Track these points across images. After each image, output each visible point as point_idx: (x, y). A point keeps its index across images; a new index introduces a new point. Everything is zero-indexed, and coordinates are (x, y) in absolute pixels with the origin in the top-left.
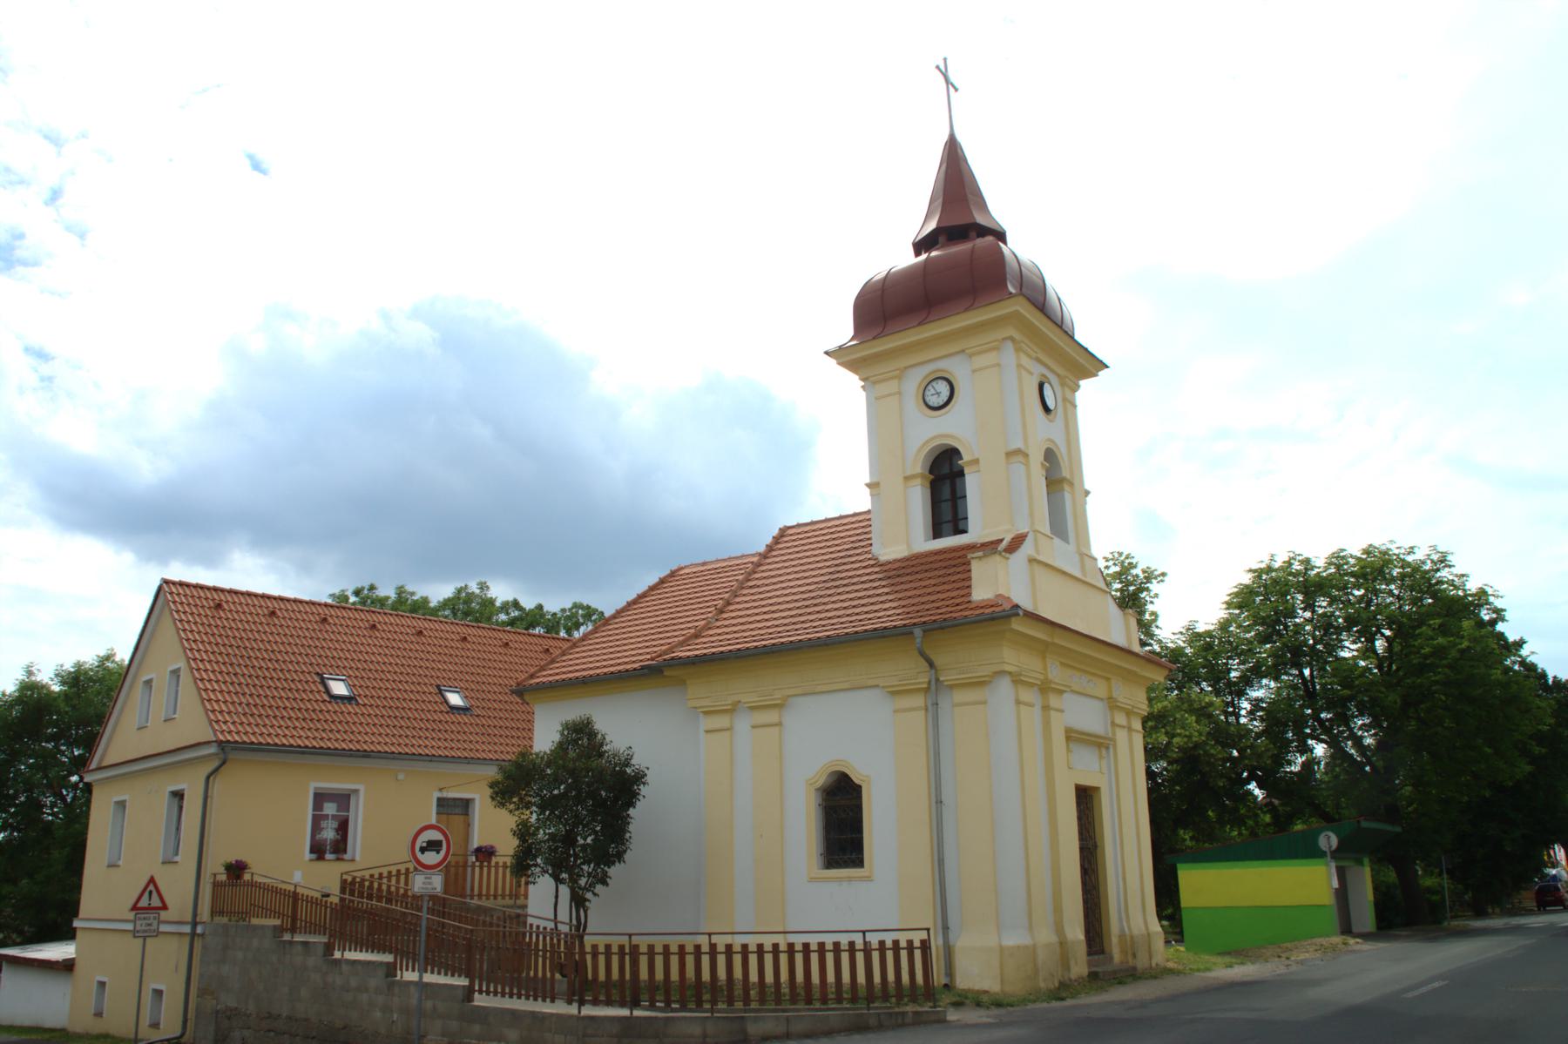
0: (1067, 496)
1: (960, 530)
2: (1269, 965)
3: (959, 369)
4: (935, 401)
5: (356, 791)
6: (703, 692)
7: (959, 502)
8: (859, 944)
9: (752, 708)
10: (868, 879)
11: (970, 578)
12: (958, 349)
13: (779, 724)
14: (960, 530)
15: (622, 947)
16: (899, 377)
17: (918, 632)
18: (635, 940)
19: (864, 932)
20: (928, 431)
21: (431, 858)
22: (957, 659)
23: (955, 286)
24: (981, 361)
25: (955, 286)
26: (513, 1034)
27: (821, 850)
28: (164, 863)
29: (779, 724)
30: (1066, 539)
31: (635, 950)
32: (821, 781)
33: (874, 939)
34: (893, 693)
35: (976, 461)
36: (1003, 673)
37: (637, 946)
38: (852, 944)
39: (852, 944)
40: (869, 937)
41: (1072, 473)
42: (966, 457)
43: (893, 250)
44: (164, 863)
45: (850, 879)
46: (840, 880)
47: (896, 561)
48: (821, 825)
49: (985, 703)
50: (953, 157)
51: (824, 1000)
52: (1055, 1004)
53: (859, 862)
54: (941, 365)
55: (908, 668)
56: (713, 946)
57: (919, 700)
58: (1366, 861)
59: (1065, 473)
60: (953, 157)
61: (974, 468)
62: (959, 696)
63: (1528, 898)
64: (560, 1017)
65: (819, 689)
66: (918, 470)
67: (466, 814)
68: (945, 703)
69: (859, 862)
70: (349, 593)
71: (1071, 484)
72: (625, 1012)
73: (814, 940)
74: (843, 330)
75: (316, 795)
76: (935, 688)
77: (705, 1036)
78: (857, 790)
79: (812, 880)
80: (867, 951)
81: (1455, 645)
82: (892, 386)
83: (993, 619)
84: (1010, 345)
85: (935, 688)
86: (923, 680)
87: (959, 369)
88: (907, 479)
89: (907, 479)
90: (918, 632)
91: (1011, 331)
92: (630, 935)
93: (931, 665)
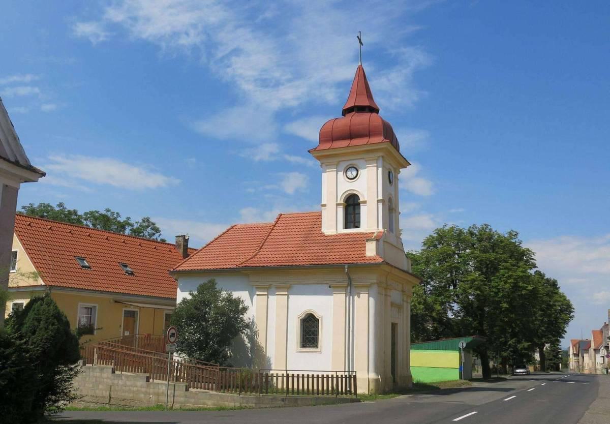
0: (394, 215)
1: (357, 226)
2: (161, 385)
4: (351, 176)
5: (95, 307)
7: (357, 216)
8: (335, 376)
12: (362, 157)
14: (357, 226)
19: (336, 372)
21: (172, 339)
30: (393, 232)
33: (290, 373)
38: (332, 376)
39: (332, 376)
40: (338, 373)
41: (396, 207)
42: (361, 199)
47: (331, 236)
51: (328, 393)
52: (383, 400)
53: (317, 346)
54: (354, 162)
56: (337, 376)
58: (471, 352)
59: (394, 206)
65: (310, 282)
66: (342, 202)
67: (134, 317)
69: (317, 346)
71: (395, 211)
75: (166, 315)
79: (298, 352)
88: (338, 205)
89: (338, 205)
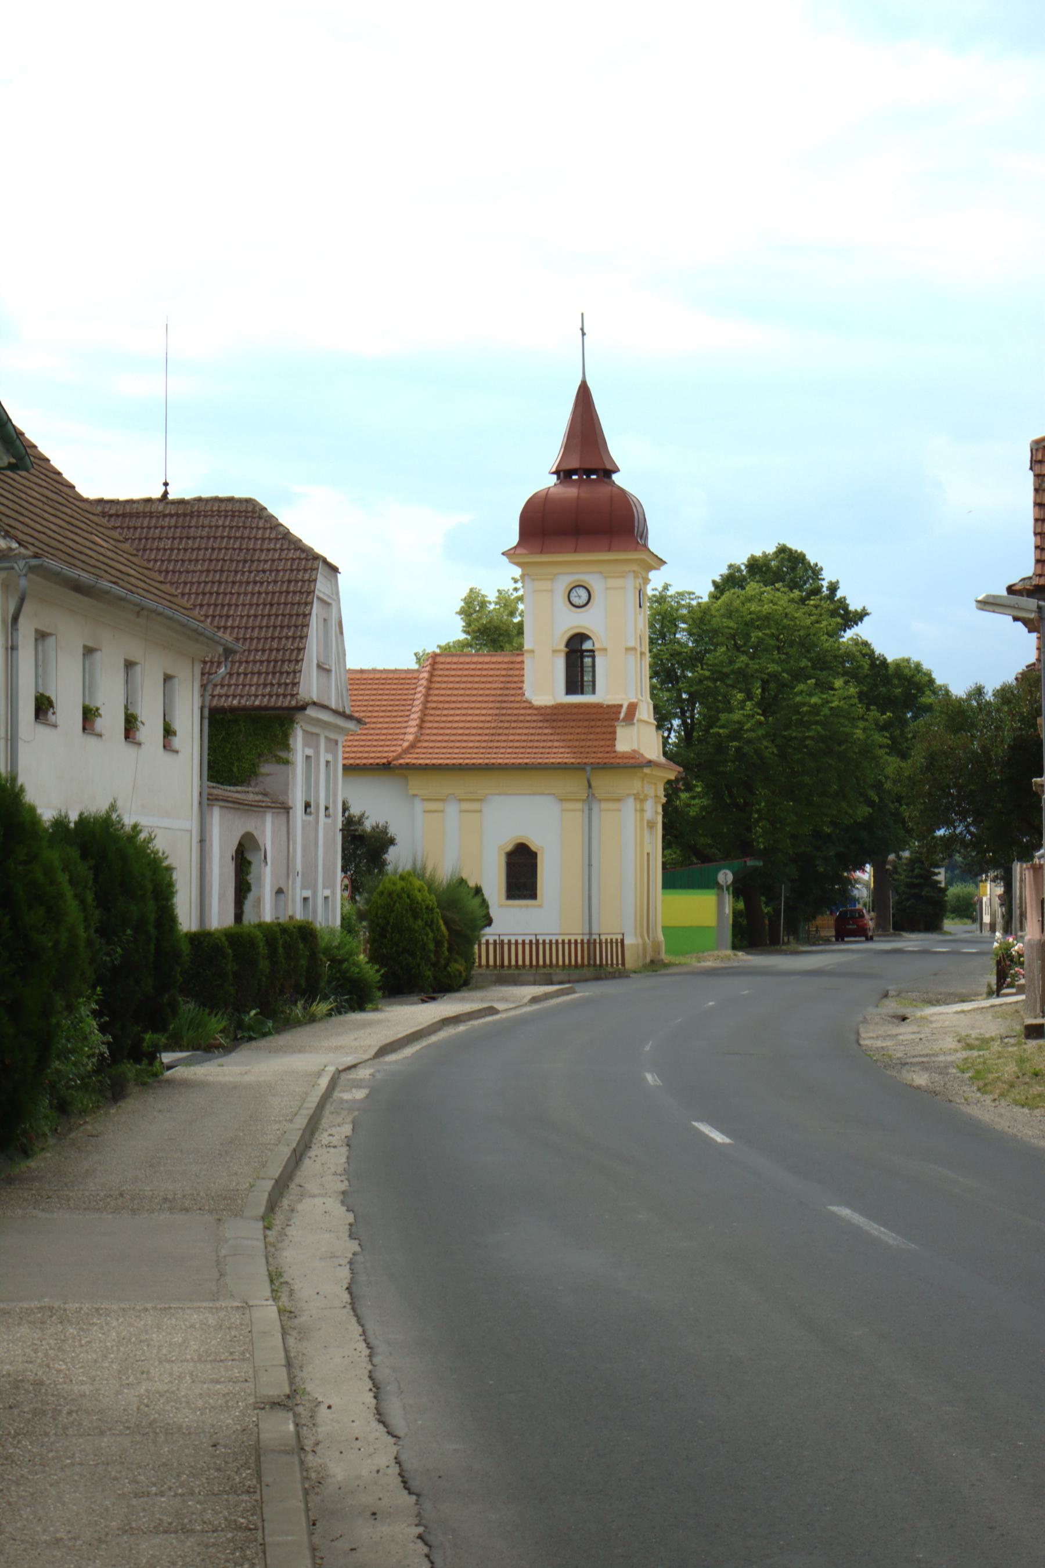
6: (417, 785)
9: (460, 800)
10: (540, 906)
11: (522, 682)
13: (480, 811)
15: (495, 941)
16: (552, 580)
17: (588, 768)
18: (502, 937)
22: (604, 784)
31: (502, 942)
32: (509, 848)
34: (562, 800)
35: (605, 650)
36: (629, 795)
45: (527, 906)
46: (521, 906)
48: (699, 891)
50: (584, 397)
53: (533, 896)
55: (574, 785)
57: (579, 806)
60: (584, 397)
62: (604, 805)
63: (826, 924)
68: (595, 806)
69: (533, 896)
70: (861, 901)
74: (513, 537)
76: (590, 798)
78: (534, 855)
79: (501, 906)
80: (601, 943)
81: (828, 702)
82: (546, 585)
83: (635, 767)
84: (632, 575)
85: (590, 798)
88: (554, 651)
89: (554, 651)
90: (588, 768)
91: (635, 568)
93: (590, 786)
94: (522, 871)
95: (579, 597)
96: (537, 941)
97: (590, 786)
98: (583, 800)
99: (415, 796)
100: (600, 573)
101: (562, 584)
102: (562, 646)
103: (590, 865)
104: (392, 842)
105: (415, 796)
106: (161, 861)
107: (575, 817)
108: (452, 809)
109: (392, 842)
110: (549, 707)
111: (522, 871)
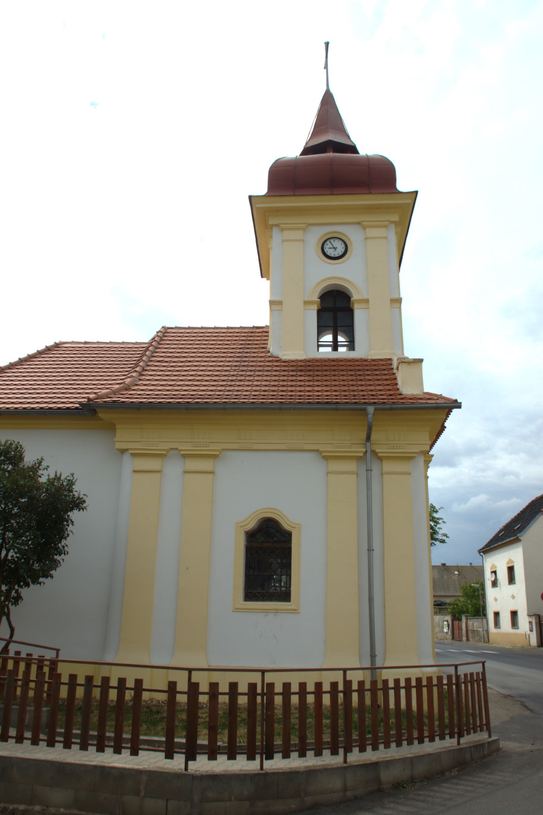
3: (354, 235)
6: (126, 436)
9: (184, 456)
10: (295, 611)
16: (304, 230)
17: (371, 409)
18: (269, 678)
20: (323, 274)
22: (386, 438)
23: (332, 182)
24: (371, 232)
25: (332, 182)
26: (59, 796)
27: (244, 586)
28: (421, 361)
29: (212, 473)
32: (251, 525)
34: (326, 458)
35: (367, 301)
37: (271, 686)
43: (292, 145)
44: (421, 361)
49: (410, 474)
50: (328, 101)
55: (345, 438)
57: (352, 466)
60: (328, 101)
61: (364, 305)
62: (388, 466)
64: (155, 776)
65: (255, 447)
69: (285, 596)
72: (253, 766)
73: (36, 653)
76: (369, 457)
77: (345, 789)
78: (287, 536)
79: (237, 610)
86: (360, 450)
87: (354, 235)
88: (306, 303)
92: (263, 672)
94: (268, 559)
95: (335, 248)
96: (348, 684)
97: (368, 438)
98: (359, 459)
99: (123, 451)
100: (359, 223)
101: (315, 237)
102: (315, 298)
103: (370, 550)
104: (78, 504)
105: (123, 451)
106: (378, 687)
107: (347, 481)
108: (173, 469)
109: (78, 504)
110: (301, 361)
111: (268, 559)
